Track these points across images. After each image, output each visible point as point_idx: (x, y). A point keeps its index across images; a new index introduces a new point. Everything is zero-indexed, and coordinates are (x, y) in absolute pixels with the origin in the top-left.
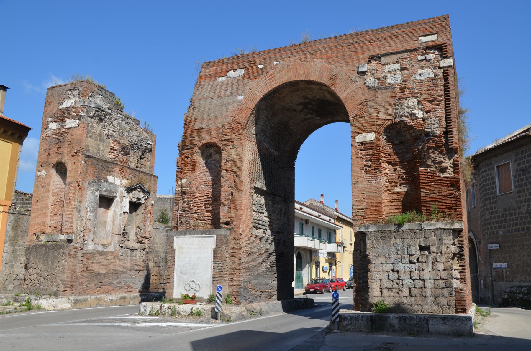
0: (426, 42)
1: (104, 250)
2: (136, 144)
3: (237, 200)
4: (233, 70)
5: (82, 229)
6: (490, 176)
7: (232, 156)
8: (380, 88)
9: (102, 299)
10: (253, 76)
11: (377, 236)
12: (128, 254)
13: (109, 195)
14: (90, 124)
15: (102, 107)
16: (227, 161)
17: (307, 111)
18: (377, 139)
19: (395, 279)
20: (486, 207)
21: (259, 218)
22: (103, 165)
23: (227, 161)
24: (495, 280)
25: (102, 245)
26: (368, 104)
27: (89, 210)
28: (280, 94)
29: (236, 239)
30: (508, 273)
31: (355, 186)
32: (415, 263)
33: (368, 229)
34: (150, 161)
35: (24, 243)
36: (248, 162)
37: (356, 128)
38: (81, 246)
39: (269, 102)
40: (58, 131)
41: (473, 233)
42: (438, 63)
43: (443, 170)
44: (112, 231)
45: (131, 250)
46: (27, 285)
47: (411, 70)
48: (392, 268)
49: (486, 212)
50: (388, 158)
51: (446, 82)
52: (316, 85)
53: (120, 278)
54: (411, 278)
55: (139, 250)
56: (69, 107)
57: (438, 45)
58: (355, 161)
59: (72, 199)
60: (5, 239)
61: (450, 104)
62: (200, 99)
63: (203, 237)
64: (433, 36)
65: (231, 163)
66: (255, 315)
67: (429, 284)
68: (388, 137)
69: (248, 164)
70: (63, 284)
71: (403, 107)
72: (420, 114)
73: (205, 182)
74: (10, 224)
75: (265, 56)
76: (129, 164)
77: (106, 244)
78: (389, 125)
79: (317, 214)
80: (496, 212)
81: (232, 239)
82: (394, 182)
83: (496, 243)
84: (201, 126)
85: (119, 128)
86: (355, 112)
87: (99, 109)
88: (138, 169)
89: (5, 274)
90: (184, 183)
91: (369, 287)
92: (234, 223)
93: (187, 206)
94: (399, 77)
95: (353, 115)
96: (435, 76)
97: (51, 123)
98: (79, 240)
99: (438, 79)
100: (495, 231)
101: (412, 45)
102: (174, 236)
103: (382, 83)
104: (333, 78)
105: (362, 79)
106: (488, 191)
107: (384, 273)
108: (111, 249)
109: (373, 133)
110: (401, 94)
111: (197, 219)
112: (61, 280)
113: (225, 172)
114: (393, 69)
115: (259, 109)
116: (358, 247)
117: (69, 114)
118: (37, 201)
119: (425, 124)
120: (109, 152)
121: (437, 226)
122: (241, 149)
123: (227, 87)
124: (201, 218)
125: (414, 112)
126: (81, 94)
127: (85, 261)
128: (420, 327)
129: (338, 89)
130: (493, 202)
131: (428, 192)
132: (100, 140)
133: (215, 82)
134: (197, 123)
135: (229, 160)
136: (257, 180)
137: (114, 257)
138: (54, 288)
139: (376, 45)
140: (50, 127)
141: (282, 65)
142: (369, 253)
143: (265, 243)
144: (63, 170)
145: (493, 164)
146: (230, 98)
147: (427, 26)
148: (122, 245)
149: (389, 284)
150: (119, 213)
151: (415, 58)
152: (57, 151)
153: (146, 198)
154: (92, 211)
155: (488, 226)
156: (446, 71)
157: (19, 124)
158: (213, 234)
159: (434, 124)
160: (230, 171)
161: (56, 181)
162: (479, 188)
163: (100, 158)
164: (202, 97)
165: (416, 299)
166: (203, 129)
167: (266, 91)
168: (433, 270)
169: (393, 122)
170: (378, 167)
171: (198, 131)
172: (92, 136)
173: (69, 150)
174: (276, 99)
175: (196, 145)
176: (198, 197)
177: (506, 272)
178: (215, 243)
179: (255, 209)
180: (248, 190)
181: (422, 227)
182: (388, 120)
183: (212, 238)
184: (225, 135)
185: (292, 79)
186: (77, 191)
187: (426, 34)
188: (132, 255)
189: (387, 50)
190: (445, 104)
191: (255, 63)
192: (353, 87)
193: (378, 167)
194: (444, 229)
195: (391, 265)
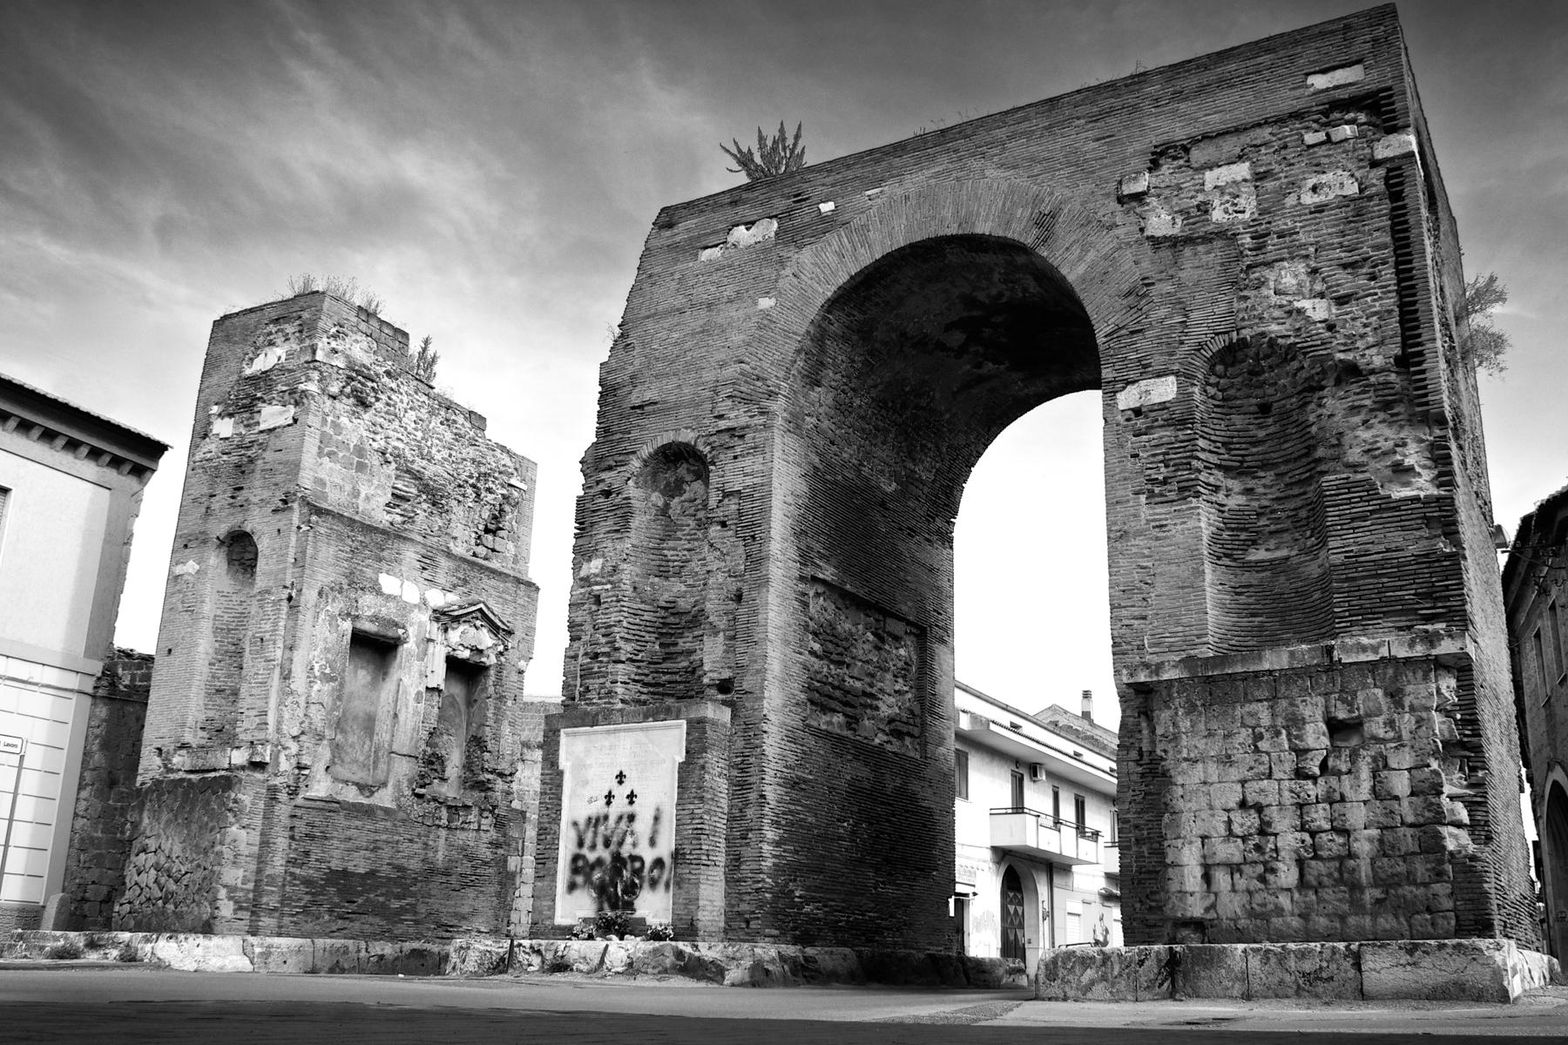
0: (1327, 89)
2: (473, 486)
3: (755, 613)
4: (745, 224)
7: (741, 478)
8: (1189, 241)
9: (350, 949)
10: (803, 237)
11: (1188, 695)
12: (440, 819)
13: (383, 631)
14: (329, 419)
15: (369, 369)
16: (724, 497)
17: (981, 349)
18: (1184, 396)
21: (830, 680)
23: (727, 495)
25: (357, 784)
26: (1154, 290)
27: (317, 674)
31: (1118, 545)
32: (1314, 778)
33: (1157, 675)
37: (1117, 367)
39: (854, 316)
40: (237, 440)
42: (1367, 151)
45: (449, 807)
46: (129, 903)
47: (1286, 177)
48: (1238, 797)
50: (1222, 457)
51: (1394, 205)
53: (413, 895)
56: (271, 370)
59: (268, 641)
62: (648, 317)
63: (647, 729)
65: (737, 501)
69: (790, 505)
70: (230, 898)
71: (1264, 291)
72: (1318, 310)
73: (662, 569)
74: (98, 731)
75: (838, 176)
76: (451, 545)
77: (370, 783)
78: (1219, 351)
79: (1070, 748)
82: (1246, 530)
84: (648, 396)
86: (1113, 320)
87: (358, 373)
92: (745, 686)
93: (603, 640)
95: (1108, 330)
96: (1361, 191)
97: (219, 420)
99: (1370, 198)
101: (1286, 100)
102: (562, 731)
103: (1194, 224)
105: (1133, 218)
107: (1213, 816)
108: (384, 798)
109: (1172, 378)
110: (1254, 253)
111: (634, 681)
112: (225, 886)
113: (720, 531)
114: (1229, 179)
116: (1131, 740)
117: (270, 389)
118: (170, 651)
119: (1335, 337)
120: (387, 505)
122: (768, 456)
124: (648, 679)
125: (1297, 305)
126: (306, 330)
128: (1332, 978)
129: (1061, 252)
131: (1352, 551)
132: (361, 467)
134: (637, 389)
135: (732, 494)
137: (395, 825)
140: (214, 432)
141: (890, 197)
143: (850, 757)
146: (735, 306)
148: (422, 791)
149: (1230, 851)
150: (413, 692)
151: (1295, 141)
152: (232, 501)
153: (501, 648)
154: (328, 678)
156: (1395, 172)
158: (677, 718)
159: (1362, 336)
163: (357, 518)
165: (1322, 893)
166: (656, 403)
167: (843, 278)
168: (1376, 798)
170: (1190, 483)
171: (639, 411)
172: (335, 453)
174: (877, 304)
175: (634, 453)
176: (639, 612)
182: (1217, 334)
183: (676, 732)
184: (721, 417)
188: (453, 825)
189: (1207, 123)
190: (1398, 273)
192: (1105, 243)
193: (1190, 483)
194: (1407, 660)
195: (1238, 787)
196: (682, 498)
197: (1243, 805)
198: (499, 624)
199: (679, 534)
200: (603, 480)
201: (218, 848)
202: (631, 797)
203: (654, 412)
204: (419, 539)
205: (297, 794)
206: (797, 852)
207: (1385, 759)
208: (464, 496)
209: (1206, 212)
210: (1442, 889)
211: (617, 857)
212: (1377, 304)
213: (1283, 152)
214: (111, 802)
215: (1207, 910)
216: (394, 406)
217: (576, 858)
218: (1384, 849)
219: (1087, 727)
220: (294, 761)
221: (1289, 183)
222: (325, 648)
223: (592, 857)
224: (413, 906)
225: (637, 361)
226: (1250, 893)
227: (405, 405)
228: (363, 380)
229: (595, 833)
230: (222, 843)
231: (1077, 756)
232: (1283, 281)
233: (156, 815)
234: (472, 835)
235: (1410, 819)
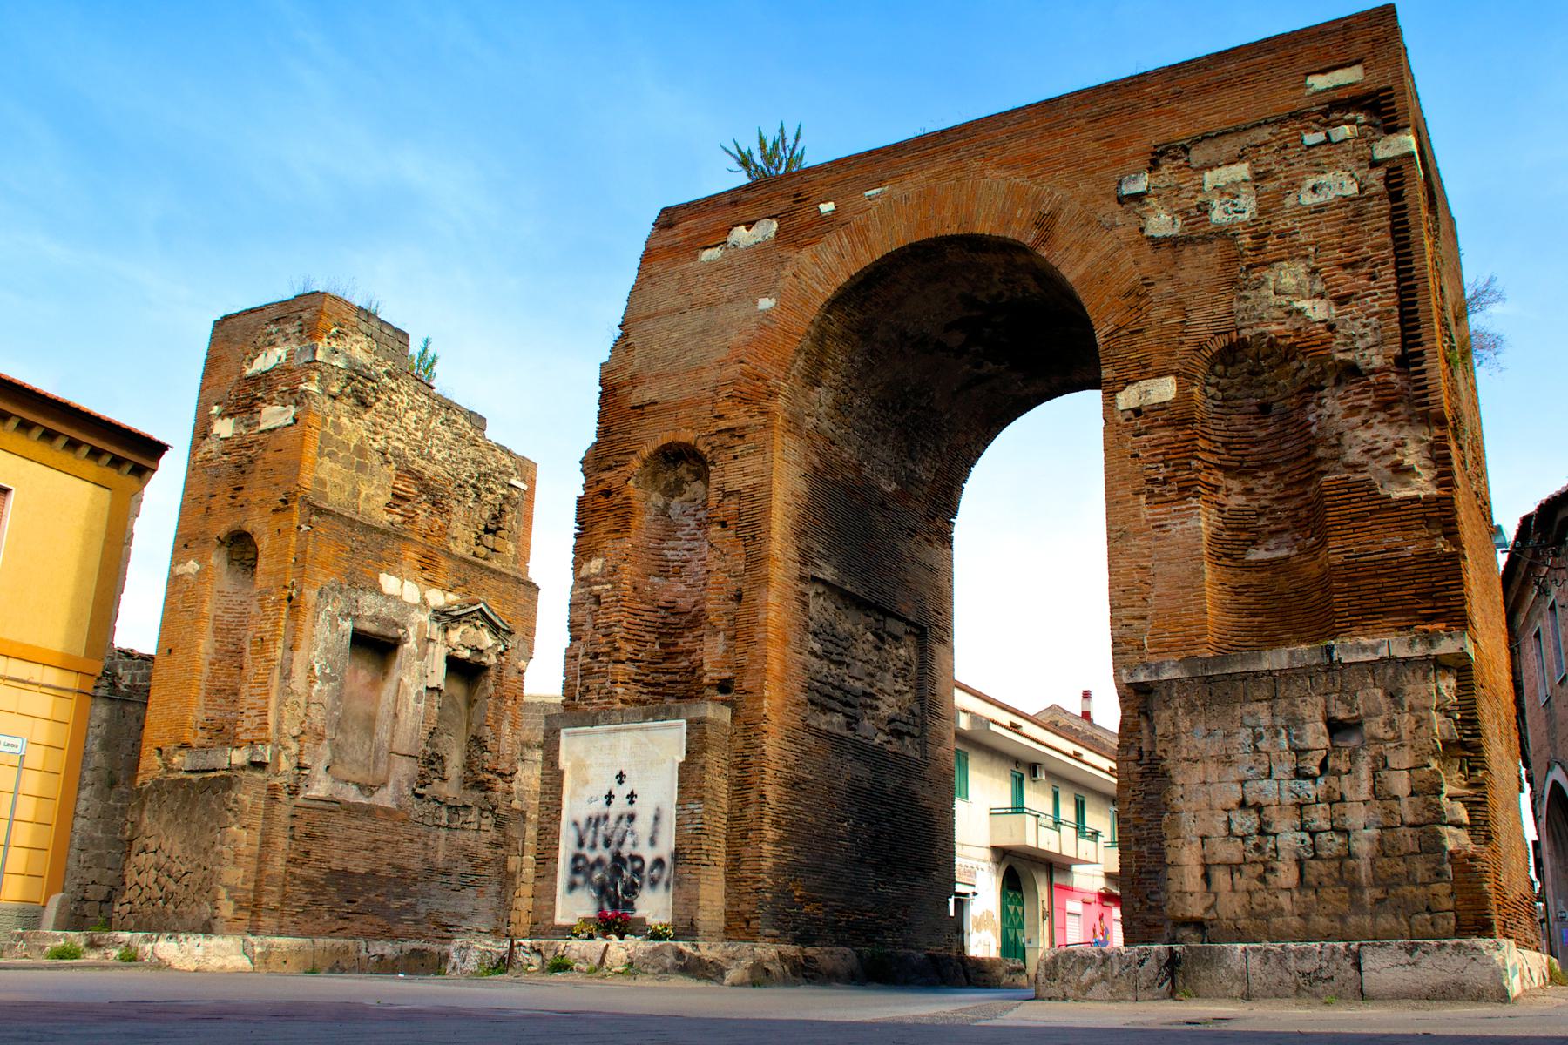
0: (1327, 90)
1: (365, 801)
2: (474, 486)
3: (754, 613)
5: (295, 731)
7: (741, 478)
8: (1189, 241)
13: (382, 631)
14: (330, 419)
18: (1184, 396)
19: (1251, 831)
21: (830, 680)
23: (727, 495)
25: (357, 784)
29: (752, 733)
32: (1314, 778)
34: (516, 540)
38: (291, 782)
41: (1563, 768)
43: (1401, 471)
44: (390, 746)
45: (450, 807)
46: (130, 903)
47: (1285, 177)
48: (1238, 797)
50: (1221, 457)
51: (1394, 205)
52: (995, 253)
53: (413, 895)
54: (1302, 825)
55: (475, 811)
56: (271, 370)
57: (1370, 95)
58: (1118, 470)
60: (81, 777)
61: (1411, 270)
62: (648, 317)
63: (647, 729)
64: (1348, 69)
66: (812, 977)
67: (1363, 844)
68: (1219, 391)
69: (790, 505)
70: (230, 898)
71: (1264, 292)
72: (1318, 310)
73: (662, 569)
74: (98, 731)
76: (452, 545)
79: (1070, 747)
81: (740, 734)
84: (649, 396)
85: (420, 434)
86: (1112, 320)
90: (597, 571)
91: (1168, 861)
92: (745, 686)
94: (1248, 204)
95: (1108, 329)
96: (1361, 191)
98: (285, 765)
99: (1370, 198)
101: (1286, 101)
102: (562, 731)
104: (1045, 223)
105: (1132, 218)
107: (1213, 816)
108: (385, 798)
109: (1171, 379)
110: (1254, 253)
111: (634, 681)
112: (225, 886)
117: (271, 388)
118: (170, 651)
120: (388, 505)
121: (1383, 652)
122: (768, 456)
123: (727, 274)
125: (1297, 305)
126: (306, 330)
127: (302, 828)
129: (1060, 252)
131: (1351, 551)
132: (361, 467)
133: (691, 264)
134: (637, 389)
135: (731, 494)
137: (395, 825)
139: (1174, 111)
140: (215, 432)
142: (1165, 751)
143: (850, 757)
144: (248, 556)
146: (735, 306)
147: (1328, 43)
148: (422, 791)
149: (1230, 851)
150: (413, 691)
151: (1294, 141)
156: (1395, 172)
159: (1362, 336)
160: (733, 526)
161: (226, 590)
164: (653, 311)
166: (656, 403)
167: (843, 279)
169: (1234, 341)
170: (1190, 483)
172: (334, 453)
173: (266, 494)
174: (877, 304)
176: (640, 612)
178: (684, 743)
179: (816, 647)
181: (1335, 659)
182: (1217, 334)
183: (676, 731)
184: (721, 417)
185: (922, 236)
186: (284, 616)
187: (1327, 66)
188: (453, 825)
189: (1207, 123)
190: (1398, 273)
191: (808, 199)
193: (1190, 483)
194: (1407, 660)
195: (1238, 787)
196: (682, 498)
197: (1243, 804)
198: (500, 624)
199: (679, 534)
201: (218, 848)
202: (632, 797)
205: (297, 794)
207: (1385, 759)
209: (1206, 212)
210: (1442, 889)
211: (617, 857)
212: (1377, 304)
213: (1282, 152)
214: (111, 802)
215: (1207, 909)
217: (576, 858)
218: (1383, 849)
220: (294, 761)
221: (1288, 183)
222: (325, 648)
223: (592, 856)
226: (1249, 892)
227: (405, 405)
229: (596, 833)
230: (222, 843)
232: (1283, 281)
234: (472, 835)
235: (1410, 819)
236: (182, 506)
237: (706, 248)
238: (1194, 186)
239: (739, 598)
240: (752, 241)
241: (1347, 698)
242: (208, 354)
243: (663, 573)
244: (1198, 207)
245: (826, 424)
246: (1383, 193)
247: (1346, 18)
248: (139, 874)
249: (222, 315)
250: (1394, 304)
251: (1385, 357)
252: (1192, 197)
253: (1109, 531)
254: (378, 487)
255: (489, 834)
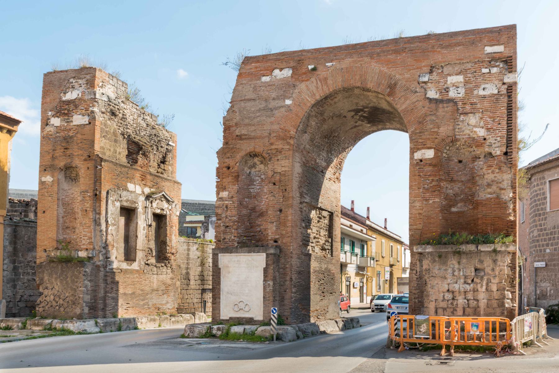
0: (491, 53)
1: (129, 268)
2: (156, 145)
6: (542, 191)
7: (280, 168)
20: (535, 224)
22: (122, 171)
24: (539, 299)
28: (332, 100)
29: (287, 257)
30: (552, 292)
32: (470, 284)
35: (26, 259)
36: (297, 175)
49: (535, 228)
56: (75, 99)
61: (511, 123)
62: (241, 101)
63: (252, 255)
70: (87, 306)
80: (545, 230)
83: (542, 261)
84: (244, 132)
88: (159, 174)
89: (7, 295)
91: (425, 306)
96: (498, 92)
100: (542, 248)
106: (538, 207)
109: (433, 150)
115: (309, 116)
130: (542, 218)
133: (258, 82)
134: (239, 129)
136: (307, 194)
138: (78, 311)
139: (439, 52)
145: (546, 178)
149: (443, 305)
155: (536, 244)
157: (12, 119)
162: (529, 202)
172: (106, 136)
174: (328, 105)
177: (550, 291)
180: (297, 205)
181: (479, 249)
190: (507, 124)
196: (256, 170)
199: (255, 183)
200: (226, 162)
203: (246, 139)
204: (140, 168)
206: (300, 294)
207: (490, 280)
208: (153, 149)
209: (448, 92)
212: (500, 133)
213: (475, 73)
214: (16, 264)
216: (126, 115)
219: (352, 213)
220: (105, 256)
221: (475, 86)
224: (147, 303)
225: (237, 117)
227: (129, 114)
228: (114, 106)
231: (351, 227)
232: (471, 121)
233: (50, 275)
234: (165, 276)
235: (496, 298)
236: (41, 153)
237: (264, 76)
238: (444, 81)
239: (281, 211)
240: (282, 77)
241: (481, 262)
242: (43, 88)
243: (249, 197)
244: (445, 89)
245: (308, 146)
246: (506, 94)
247: (500, 27)
248: (46, 297)
249: (48, 71)
250: (505, 134)
251: (501, 151)
252: (444, 85)
253: (410, 200)
254: (123, 149)
255: (170, 275)
